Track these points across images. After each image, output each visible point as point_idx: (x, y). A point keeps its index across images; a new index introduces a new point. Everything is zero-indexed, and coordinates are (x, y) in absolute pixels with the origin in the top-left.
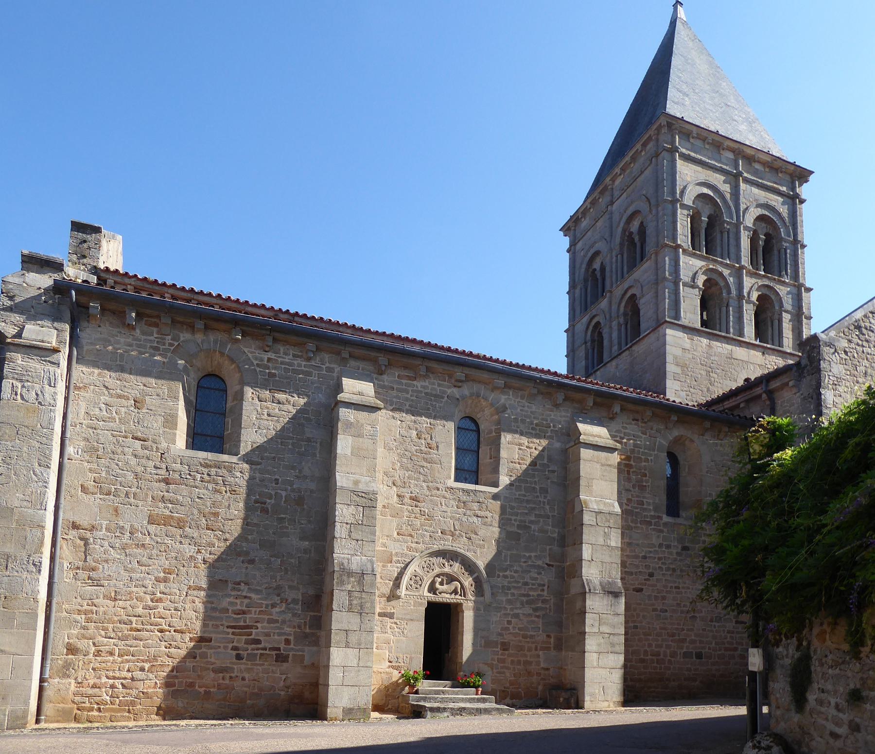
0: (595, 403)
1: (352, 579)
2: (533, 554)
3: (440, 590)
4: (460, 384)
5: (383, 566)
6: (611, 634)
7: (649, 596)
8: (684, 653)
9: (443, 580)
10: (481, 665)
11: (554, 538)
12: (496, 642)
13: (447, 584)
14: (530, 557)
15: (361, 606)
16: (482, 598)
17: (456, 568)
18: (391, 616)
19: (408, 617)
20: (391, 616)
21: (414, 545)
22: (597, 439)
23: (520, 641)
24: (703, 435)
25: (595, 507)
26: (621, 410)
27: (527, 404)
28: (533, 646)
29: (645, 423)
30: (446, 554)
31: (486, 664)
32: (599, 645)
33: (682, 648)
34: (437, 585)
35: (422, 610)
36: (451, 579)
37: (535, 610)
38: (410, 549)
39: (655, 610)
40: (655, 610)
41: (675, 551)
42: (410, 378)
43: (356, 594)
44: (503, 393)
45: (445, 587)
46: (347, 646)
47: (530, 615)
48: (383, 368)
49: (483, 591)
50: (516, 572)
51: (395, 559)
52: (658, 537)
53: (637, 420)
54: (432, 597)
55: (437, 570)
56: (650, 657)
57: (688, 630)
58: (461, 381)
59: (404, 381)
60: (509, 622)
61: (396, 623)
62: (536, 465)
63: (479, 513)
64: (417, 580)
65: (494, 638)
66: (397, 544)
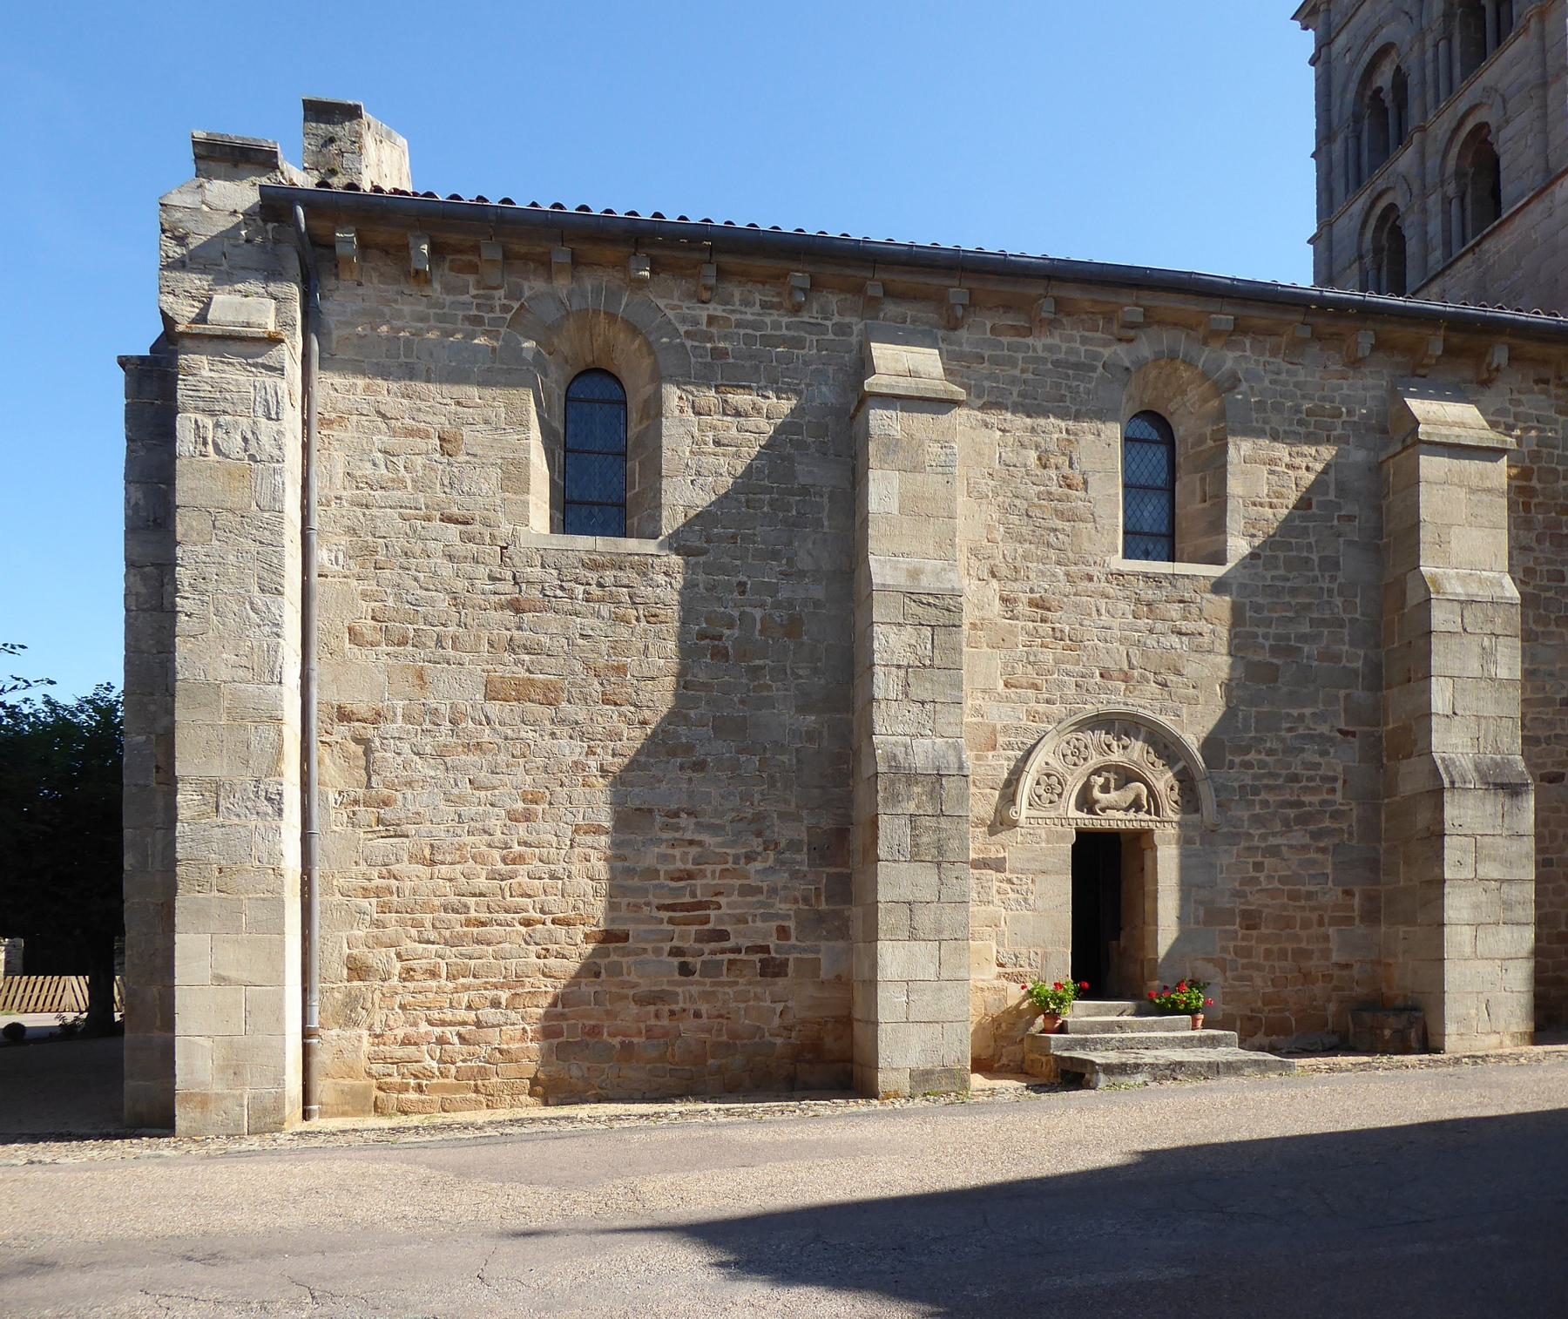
1: (917, 789)
2: (1308, 711)
3: (1103, 805)
4: (1132, 333)
5: (978, 758)
6: (1502, 881)
9: (1107, 780)
10: (1199, 964)
12: (1231, 912)
13: (1117, 789)
14: (1301, 717)
15: (939, 848)
16: (1196, 817)
17: (1136, 752)
18: (998, 865)
19: (1035, 866)
20: (998, 865)
21: (1042, 707)
25: (1460, 590)
28: (1315, 916)
30: (1112, 722)
31: (1209, 960)
32: (1476, 907)
34: (1097, 794)
35: (1067, 847)
36: (1126, 776)
38: (1033, 716)
42: (1017, 331)
43: (927, 822)
44: (1229, 345)
45: (1114, 796)
47: (1304, 848)
48: (959, 312)
49: (1198, 799)
50: (1270, 752)
51: (1001, 740)
53: (1546, 382)
54: (1086, 820)
55: (1095, 760)
59: (1005, 340)
60: (1258, 866)
61: (1010, 881)
63: (1184, 626)
64: (1052, 784)
65: (1225, 902)
66: (1006, 708)
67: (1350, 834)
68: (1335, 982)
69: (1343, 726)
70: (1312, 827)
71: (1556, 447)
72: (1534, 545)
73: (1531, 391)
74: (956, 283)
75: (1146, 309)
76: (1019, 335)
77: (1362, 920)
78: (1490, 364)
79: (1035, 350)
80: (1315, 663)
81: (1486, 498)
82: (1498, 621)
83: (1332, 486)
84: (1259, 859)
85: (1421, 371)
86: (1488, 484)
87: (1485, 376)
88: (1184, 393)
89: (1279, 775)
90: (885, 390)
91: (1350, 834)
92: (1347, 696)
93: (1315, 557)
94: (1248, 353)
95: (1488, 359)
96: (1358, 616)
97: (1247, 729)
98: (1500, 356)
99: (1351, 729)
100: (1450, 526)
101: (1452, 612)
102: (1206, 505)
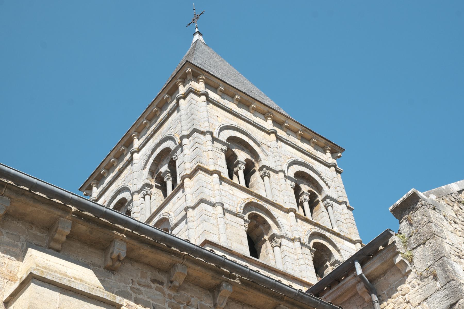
29: (177, 289)
53: (162, 283)
73: (150, 287)
87: (110, 263)
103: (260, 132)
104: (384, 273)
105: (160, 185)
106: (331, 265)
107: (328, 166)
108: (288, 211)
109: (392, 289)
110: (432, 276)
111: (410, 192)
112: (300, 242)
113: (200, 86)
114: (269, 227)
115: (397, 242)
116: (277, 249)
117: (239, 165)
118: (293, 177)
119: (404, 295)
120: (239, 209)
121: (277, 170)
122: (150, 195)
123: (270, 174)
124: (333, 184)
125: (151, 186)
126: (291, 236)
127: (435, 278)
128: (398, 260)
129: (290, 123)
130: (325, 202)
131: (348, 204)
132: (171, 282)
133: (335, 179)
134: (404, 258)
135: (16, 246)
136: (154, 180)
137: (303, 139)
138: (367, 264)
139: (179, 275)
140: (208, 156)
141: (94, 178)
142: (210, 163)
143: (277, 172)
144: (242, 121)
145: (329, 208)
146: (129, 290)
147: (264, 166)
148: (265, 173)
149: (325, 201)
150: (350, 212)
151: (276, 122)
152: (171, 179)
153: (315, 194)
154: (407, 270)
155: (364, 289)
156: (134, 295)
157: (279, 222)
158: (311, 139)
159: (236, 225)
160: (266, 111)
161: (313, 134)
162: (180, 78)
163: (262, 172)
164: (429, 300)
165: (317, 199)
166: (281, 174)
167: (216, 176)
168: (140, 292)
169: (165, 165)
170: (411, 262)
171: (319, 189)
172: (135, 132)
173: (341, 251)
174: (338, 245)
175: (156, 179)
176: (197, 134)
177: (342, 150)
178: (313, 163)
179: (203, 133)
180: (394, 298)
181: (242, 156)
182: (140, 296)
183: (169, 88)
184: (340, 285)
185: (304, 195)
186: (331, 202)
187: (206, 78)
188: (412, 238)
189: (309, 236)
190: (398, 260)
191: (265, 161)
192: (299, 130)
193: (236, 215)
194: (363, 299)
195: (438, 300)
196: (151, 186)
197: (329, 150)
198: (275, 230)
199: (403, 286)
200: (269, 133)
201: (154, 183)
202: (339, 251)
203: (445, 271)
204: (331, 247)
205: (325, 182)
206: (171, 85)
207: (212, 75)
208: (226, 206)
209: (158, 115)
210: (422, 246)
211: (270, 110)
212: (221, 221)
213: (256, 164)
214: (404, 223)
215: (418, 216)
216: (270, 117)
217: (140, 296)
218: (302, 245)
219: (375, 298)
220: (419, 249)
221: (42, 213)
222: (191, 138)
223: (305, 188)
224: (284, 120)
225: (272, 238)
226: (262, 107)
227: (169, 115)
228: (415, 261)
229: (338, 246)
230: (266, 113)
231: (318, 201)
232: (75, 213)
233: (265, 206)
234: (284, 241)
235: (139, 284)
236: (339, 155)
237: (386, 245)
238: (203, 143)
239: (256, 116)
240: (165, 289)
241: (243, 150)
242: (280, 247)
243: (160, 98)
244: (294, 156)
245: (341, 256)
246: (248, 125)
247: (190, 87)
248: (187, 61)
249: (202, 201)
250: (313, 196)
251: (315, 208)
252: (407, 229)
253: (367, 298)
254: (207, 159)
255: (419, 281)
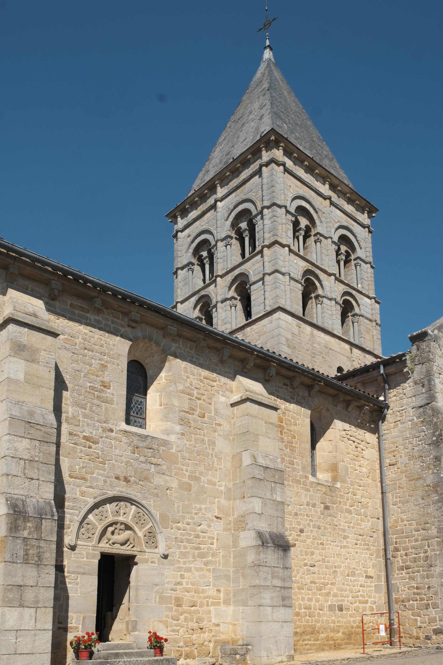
0: (255, 365)
1: (29, 524)
2: (203, 506)
4: (134, 325)
6: (281, 587)
7: (301, 551)
8: (330, 606)
10: (156, 623)
11: (222, 491)
14: (200, 509)
15: (39, 557)
19: (82, 571)
22: (260, 397)
23: (193, 597)
24: (336, 406)
25: (263, 462)
26: (277, 374)
27: (195, 356)
28: (205, 601)
29: (294, 388)
31: (161, 621)
32: (272, 598)
33: (327, 601)
35: (96, 562)
37: (206, 564)
39: (306, 565)
40: (306, 565)
41: (319, 510)
42: (83, 309)
43: (34, 543)
44: (173, 340)
46: (21, 606)
47: (201, 569)
48: (56, 293)
50: (188, 524)
52: (306, 495)
53: (287, 385)
56: (303, 610)
57: (332, 584)
58: (135, 322)
59: (77, 312)
60: (182, 576)
62: (204, 417)
63: (154, 460)
65: (169, 593)
67: (219, 563)
68: (213, 633)
69: (216, 514)
70: (204, 559)
71: (291, 412)
72: (284, 448)
73: (282, 388)
74: (56, 279)
75: (142, 315)
76: (83, 311)
77: (224, 603)
78: (269, 374)
79: (90, 320)
80: (206, 485)
81: (271, 426)
82: (276, 477)
83: (213, 410)
84: (183, 573)
85: (245, 370)
86: (271, 421)
87: (267, 378)
88: (153, 356)
89: (191, 535)
90: (21, 320)
91: (219, 563)
92: (218, 501)
93: (206, 439)
94: (181, 346)
95: (268, 372)
96: (222, 467)
97: (179, 512)
98: (273, 372)
99: (219, 516)
100: (258, 435)
101: (260, 470)
102: (162, 407)
103: (319, 197)
104: (396, 374)
105: (238, 237)
106: (351, 316)
107: (363, 226)
108: (330, 275)
109: (398, 384)
110: (421, 384)
111: (423, 330)
112: (335, 301)
113: (278, 154)
114: (316, 288)
115: (408, 360)
116: (319, 306)
117: (301, 231)
118: (337, 241)
119: (403, 390)
120: (298, 275)
121: (327, 236)
122: (230, 245)
123: (321, 240)
124: (364, 247)
125: (231, 238)
126: (329, 296)
127: (423, 386)
128: (405, 370)
129: (342, 187)
130: (356, 262)
131: (372, 264)
132: (292, 385)
133: (367, 240)
134: (410, 370)
135: (230, 373)
136: (234, 232)
137: (350, 201)
138: (387, 368)
139: (297, 382)
140: (282, 229)
141: (179, 209)
142: (283, 236)
143: (326, 238)
144: (307, 188)
145: (358, 267)
146: (274, 391)
147: (318, 233)
148: (318, 239)
149: (356, 260)
150: (372, 270)
151: (333, 187)
152: (248, 236)
153: (349, 253)
154: (409, 376)
155: (382, 380)
156: (276, 393)
157: (323, 284)
158: (356, 200)
159: (296, 289)
160: (326, 175)
161: (358, 196)
162: (264, 143)
163: (316, 238)
164: (417, 397)
165: (351, 258)
166: (329, 240)
167: (287, 249)
168: (278, 391)
169: (244, 222)
170: (413, 372)
171: (353, 249)
172: (218, 179)
173: (360, 306)
174: (359, 301)
175: (236, 231)
176: (276, 207)
177: (377, 210)
178: (353, 226)
179: (280, 207)
180: (398, 390)
181: (304, 222)
182: (279, 394)
183: (253, 149)
184: (368, 374)
185: (342, 255)
186: (360, 262)
187: (285, 145)
188: (417, 358)
189: (341, 295)
190: (405, 370)
191: (320, 228)
192: (347, 193)
193: (297, 281)
194: (380, 385)
195: (421, 398)
196: (231, 238)
197: (367, 210)
198: (320, 291)
199: (404, 384)
200: (325, 198)
201: (234, 236)
202: (359, 306)
203: (430, 384)
204: (354, 303)
205: (359, 243)
206: (256, 147)
207: (290, 142)
208: (292, 275)
209: (240, 170)
210: (421, 365)
211: (329, 175)
212: (288, 288)
213: (312, 230)
214: (415, 347)
215: (423, 345)
216: (328, 181)
217: (279, 394)
218: (336, 303)
219: (387, 387)
220: (419, 366)
221: (242, 355)
222: (270, 210)
223: (343, 248)
224: (338, 183)
225: (317, 297)
226: (323, 172)
227: (251, 177)
228: (415, 372)
229: (359, 302)
230: (324, 177)
231: (351, 260)
232: (256, 355)
233: (316, 271)
234: (325, 300)
235: (278, 387)
236: (374, 215)
237: (401, 359)
238: (279, 216)
239: (317, 181)
240: (288, 388)
241: (304, 216)
242: (321, 304)
243: (244, 156)
244: (341, 220)
245: (360, 309)
246: (311, 191)
247: (273, 158)
248: (272, 129)
249: (277, 271)
250: (348, 255)
251: (347, 265)
252: (415, 351)
253: (382, 384)
254: (281, 231)
255: (414, 385)
